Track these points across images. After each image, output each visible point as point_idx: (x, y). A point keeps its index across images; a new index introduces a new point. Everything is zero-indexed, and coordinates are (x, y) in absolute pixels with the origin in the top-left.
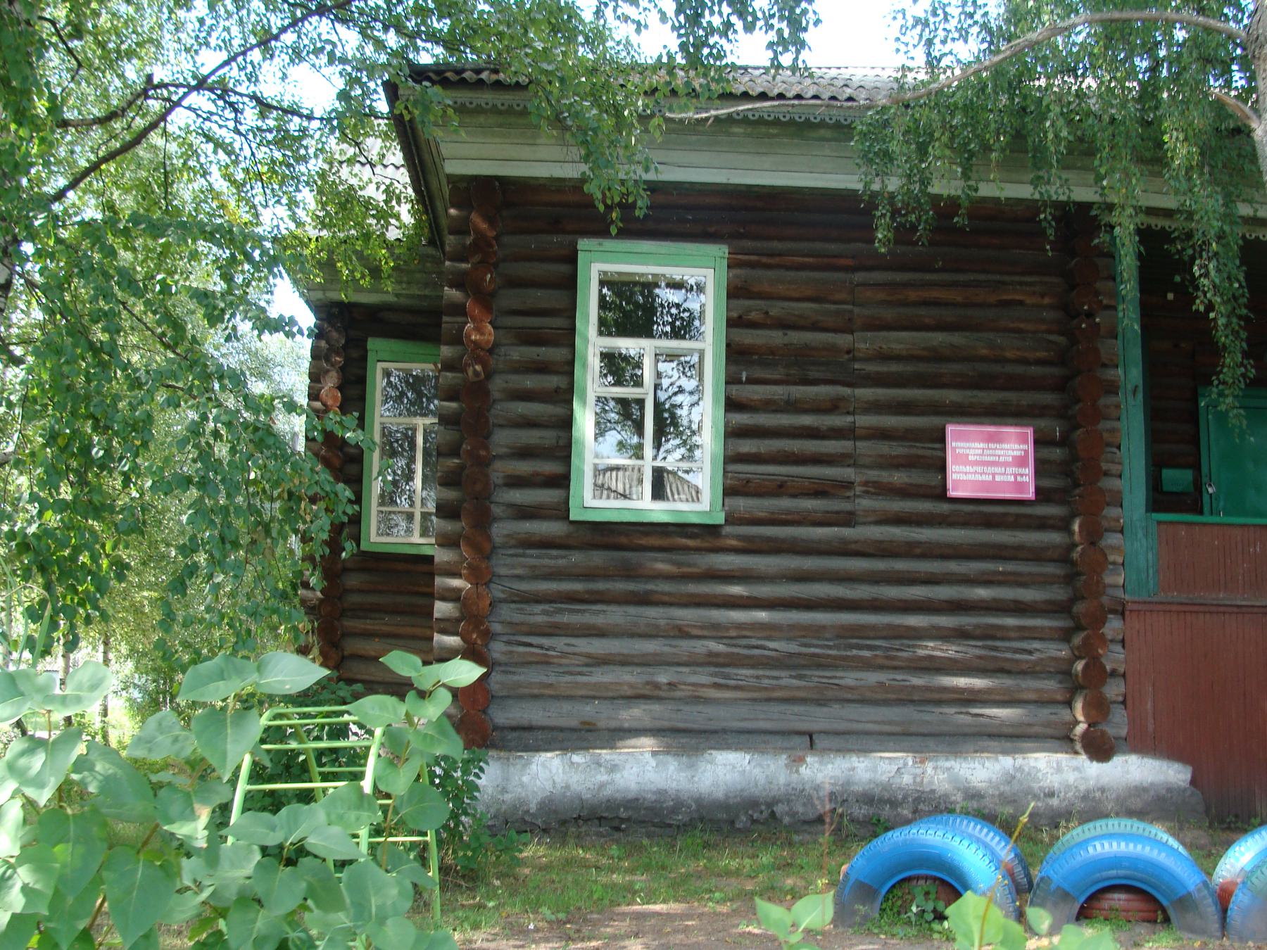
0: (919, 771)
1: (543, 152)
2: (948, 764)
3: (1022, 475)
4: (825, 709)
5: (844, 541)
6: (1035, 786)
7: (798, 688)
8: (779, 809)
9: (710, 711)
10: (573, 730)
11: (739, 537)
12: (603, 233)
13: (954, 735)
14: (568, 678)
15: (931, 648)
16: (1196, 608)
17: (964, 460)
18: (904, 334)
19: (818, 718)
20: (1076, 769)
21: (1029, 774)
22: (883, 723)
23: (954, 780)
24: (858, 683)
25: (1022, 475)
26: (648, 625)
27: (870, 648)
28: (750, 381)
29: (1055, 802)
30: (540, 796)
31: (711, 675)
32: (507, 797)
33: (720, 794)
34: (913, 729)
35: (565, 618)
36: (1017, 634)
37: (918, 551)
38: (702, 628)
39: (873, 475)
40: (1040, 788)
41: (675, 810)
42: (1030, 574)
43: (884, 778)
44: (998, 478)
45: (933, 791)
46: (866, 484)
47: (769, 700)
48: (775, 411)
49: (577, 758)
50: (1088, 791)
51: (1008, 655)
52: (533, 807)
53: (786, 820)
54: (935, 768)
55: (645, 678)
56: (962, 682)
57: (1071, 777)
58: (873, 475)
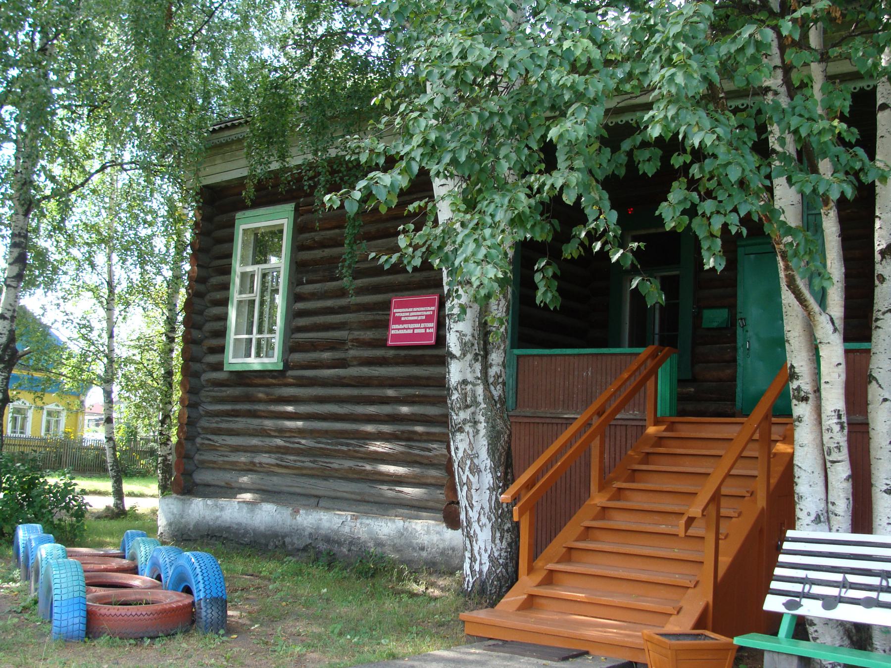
0: (353, 525)
1: (218, 168)
2: (368, 522)
3: (429, 328)
4: (325, 482)
5: (340, 378)
6: (414, 541)
7: (313, 469)
8: (287, 540)
9: (275, 479)
10: (221, 487)
11: (294, 377)
12: (246, 208)
13: (388, 504)
14: (222, 459)
15: (379, 447)
16: (537, 420)
17: (398, 321)
18: (379, 241)
19: (321, 487)
20: (438, 533)
21: (411, 533)
22: (352, 493)
23: (370, 532)
24: (340, 467)
25: (429, 328)
26: (254, 429)
27: (348, 445)
28: (309, 282)
29: (424, 554)
30: (195, 521)
31: (276, 459)
32: (183, 520)
33: (262, 528)
34: (367, 498)
35: (224, 425)
36: (276, 434)
37: (376, 382)
38: (275, 431)
39: (357, 334)
40: (417, 544)
41: (244, 535)
42: (434, 396)
43: (336, 527)
44: (416, 331)
45: (359, 538)
46: (352, 341)
47: (303, 475)
48: (319, 299)
49: (209, 502)
50: (444, 549)
51: (417, 452)
52: (191, 527)
53: (290, 547)
54: (361, 523)
55: (249, 459)
56: (391, 469)
57: (435, 538)
58: (357, 334)
